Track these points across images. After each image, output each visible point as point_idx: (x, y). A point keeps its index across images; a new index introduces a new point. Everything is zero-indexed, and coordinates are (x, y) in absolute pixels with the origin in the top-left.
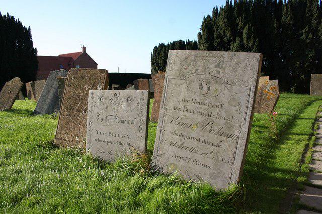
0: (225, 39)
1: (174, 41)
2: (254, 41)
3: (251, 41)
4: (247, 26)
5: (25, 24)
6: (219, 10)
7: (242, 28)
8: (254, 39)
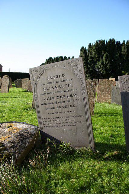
0: (94, 59)
1: (83, 50)
2: (109, 62)
3: (107, 62)
4: (106, 54)
5: (107, 39)
6: (91, 45)
7: (103, 55)
8: (109, 60)
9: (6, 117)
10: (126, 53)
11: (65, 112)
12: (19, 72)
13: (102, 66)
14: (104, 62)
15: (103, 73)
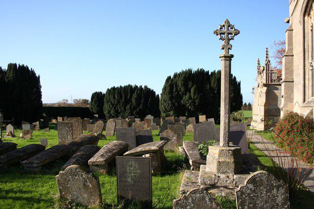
0: (180, 93)
4: (194, 87)
5: (194, 69)
7: (191, 88)
9: (210, 167)
10: (217, 85)
11: (258, 115)
12: (42, 90)
13: (190, 101)
14: (193, 96)
15: (190, 109)
